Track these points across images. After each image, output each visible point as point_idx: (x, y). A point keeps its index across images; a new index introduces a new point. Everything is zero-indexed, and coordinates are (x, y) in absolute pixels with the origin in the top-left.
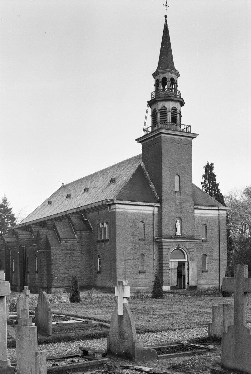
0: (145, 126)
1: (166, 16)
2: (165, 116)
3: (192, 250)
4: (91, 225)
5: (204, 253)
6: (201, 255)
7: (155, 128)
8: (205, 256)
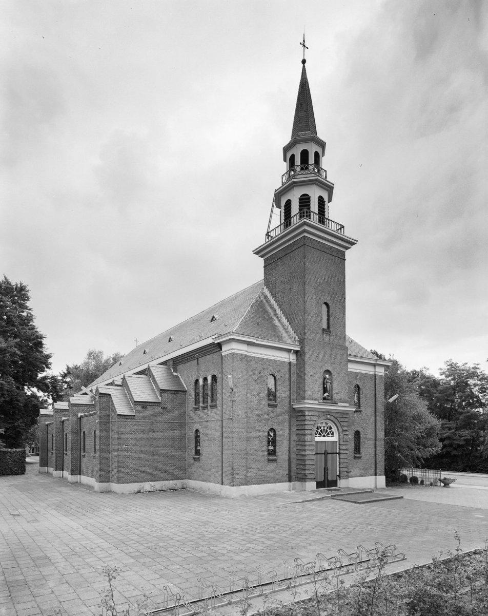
0: (269, 227)
1: (304, 62)
2: (305, 202)
3: (345, 424)
4: (183, 382)
5: (356, 429)
6: (353, 433)
7: (290, 229)
8: (357, 434)
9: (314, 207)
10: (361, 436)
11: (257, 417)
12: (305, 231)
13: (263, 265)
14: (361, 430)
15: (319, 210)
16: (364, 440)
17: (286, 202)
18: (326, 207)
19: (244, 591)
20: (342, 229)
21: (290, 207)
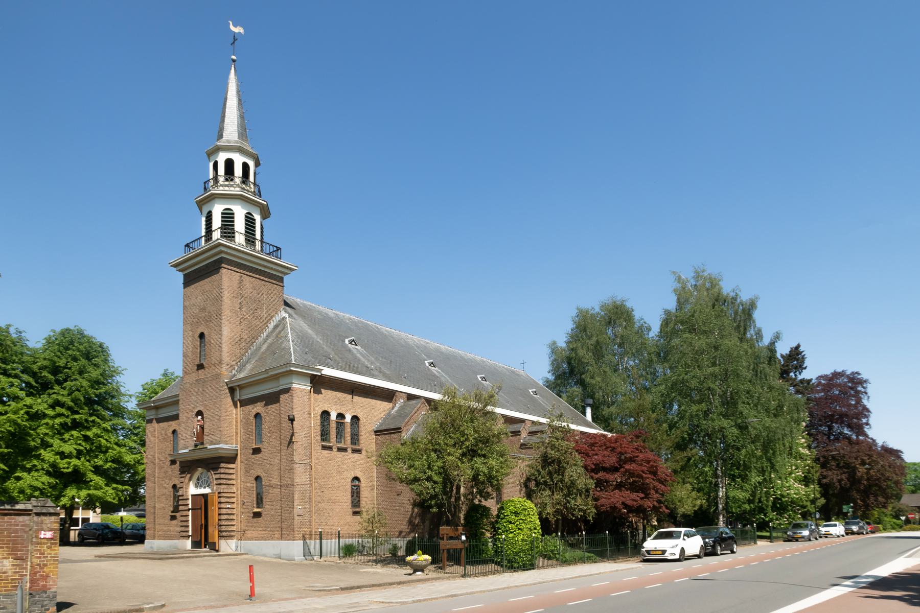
10: (263, 483)
11: (819, 435)
12: (222, 252)
13: (183, 282)
20: (279, 251)
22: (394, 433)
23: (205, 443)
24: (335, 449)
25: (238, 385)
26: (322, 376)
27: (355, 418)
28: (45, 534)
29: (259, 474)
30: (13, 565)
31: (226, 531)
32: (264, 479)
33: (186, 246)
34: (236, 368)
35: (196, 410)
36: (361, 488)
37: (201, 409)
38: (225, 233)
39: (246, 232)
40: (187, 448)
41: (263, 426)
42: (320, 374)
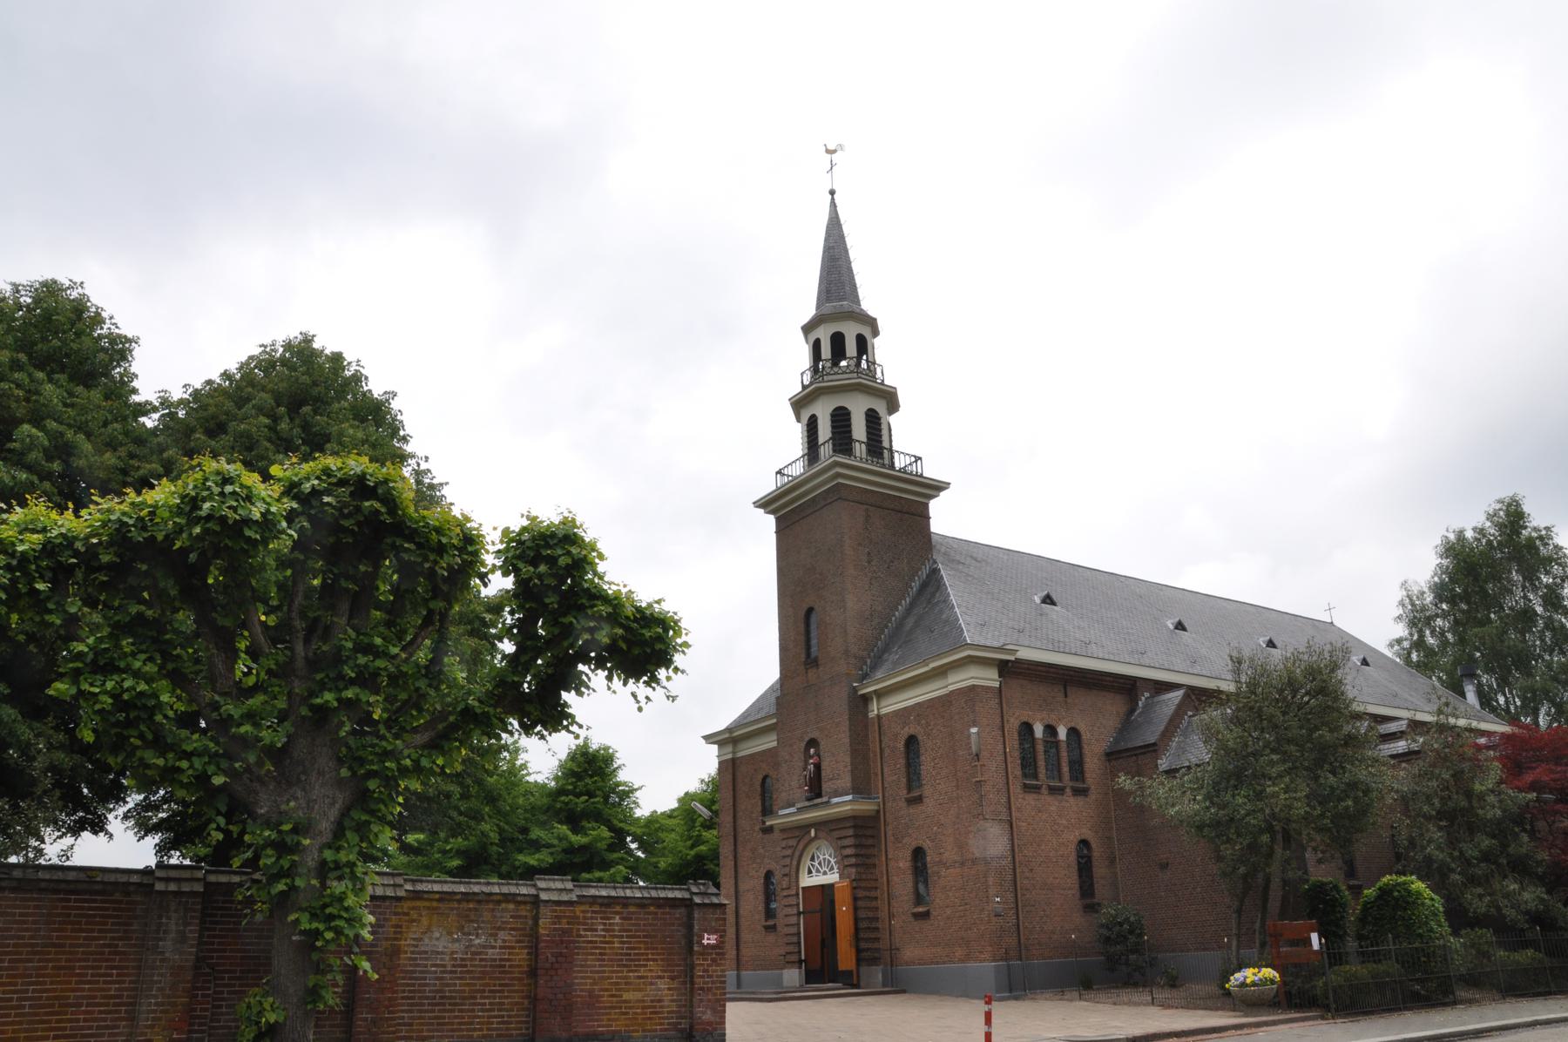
1: (832, 193)
6: (908, 854)
7: (817, 468)
8: (918, 853)
9: (859, 430)
10: (928, 859)
12: (838, 475)
13: (775, 530)
14: (927, 845)
15: (868, 433)
16: (936, 869)
17: (809, 419)
18: (884, 427)
19: (637, 705)
20: (919, 462)
21: (815, 428)
22: (1145, 753)
23: (823, 793)
24: (1044, 790)
25: (875, 691)
26: (1018, 661)
27: (1073, 732)
28: (708, 939)
29: (920, 843)
30: (669, 989)
31: (868, 949)
32: (929, 852)
33: (777, 473)
34: (869, 661)
35: (807, 739)
36: (1094, 860)
37: (815, 735)
38: (841, 445)
39: (868, 438)
40: (793, 806)
41: (923, 758)
42: (1012, 658)
